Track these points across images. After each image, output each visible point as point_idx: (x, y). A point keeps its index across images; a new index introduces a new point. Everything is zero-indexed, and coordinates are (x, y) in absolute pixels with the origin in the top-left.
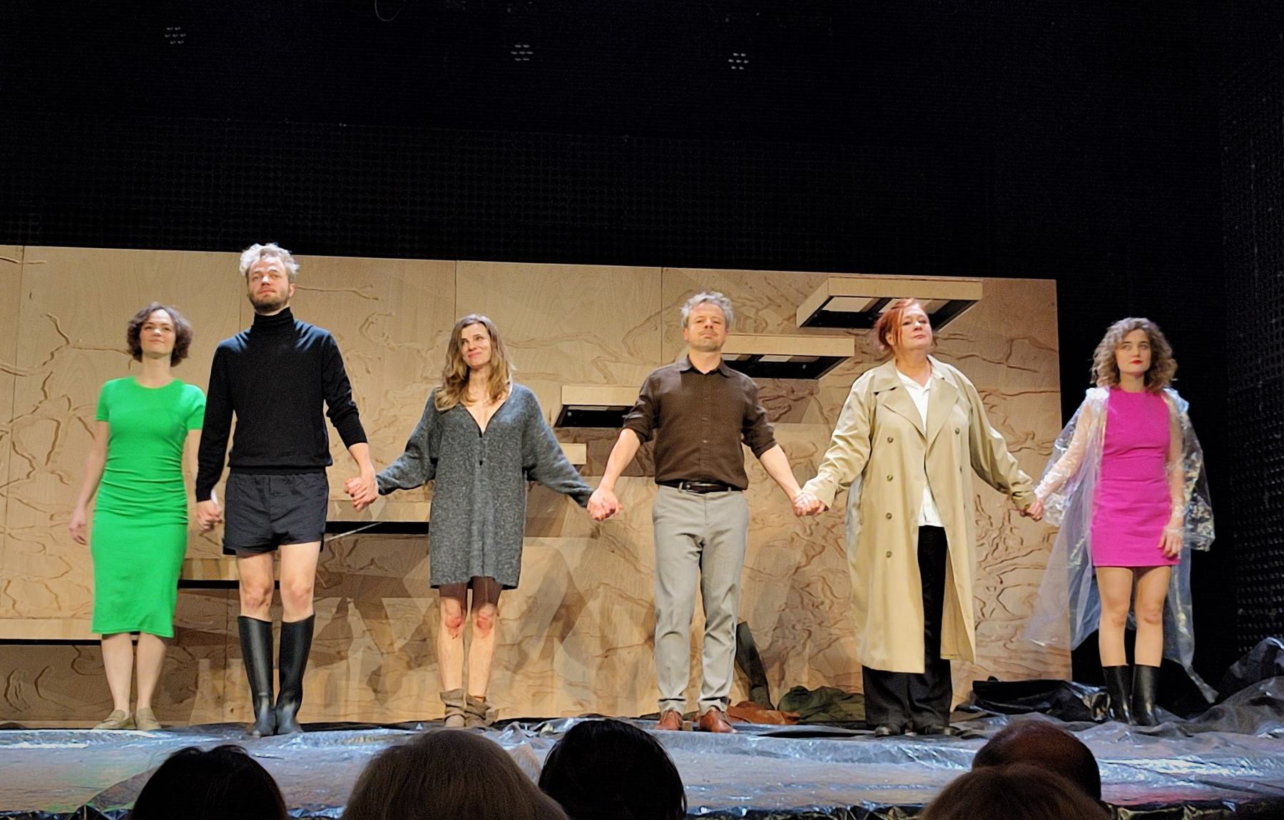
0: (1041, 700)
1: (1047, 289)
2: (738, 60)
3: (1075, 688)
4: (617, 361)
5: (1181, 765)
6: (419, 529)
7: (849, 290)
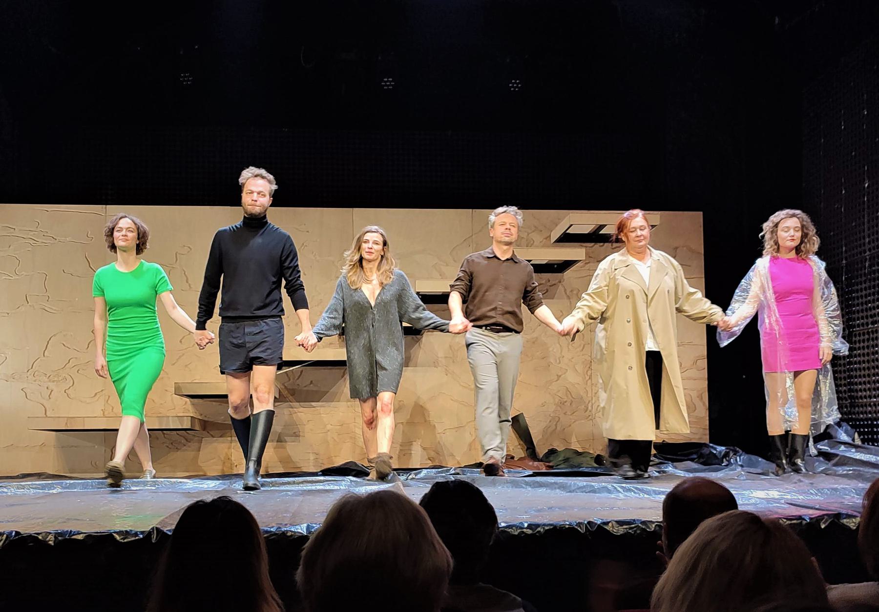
0: (692, 454)
1: (697, 217)
2: (515, 85)
3: (712, 447)
4: (447, 265)
5: (774, 494)
6: (341, 363)
7: (583, 221)
